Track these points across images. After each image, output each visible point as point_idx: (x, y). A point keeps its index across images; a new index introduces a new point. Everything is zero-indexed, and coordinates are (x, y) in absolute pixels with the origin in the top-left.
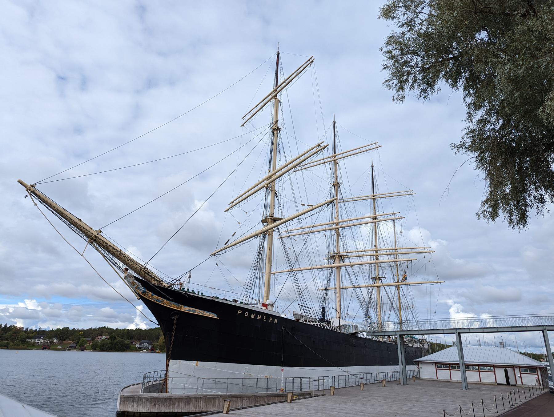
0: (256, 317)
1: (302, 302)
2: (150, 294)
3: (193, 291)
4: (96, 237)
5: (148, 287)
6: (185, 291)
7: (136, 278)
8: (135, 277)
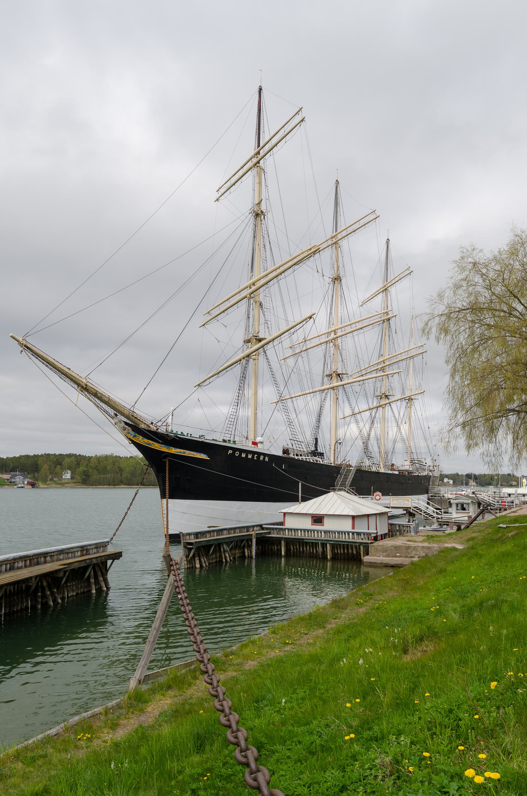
0: (247, 456)
1: (293, 436)
2: (141, 438)
3: (182, 433)
4: (86, 385)
5: (135, 429)
6: (174, 434)
7: (126, 423)
8: (125, 422)
